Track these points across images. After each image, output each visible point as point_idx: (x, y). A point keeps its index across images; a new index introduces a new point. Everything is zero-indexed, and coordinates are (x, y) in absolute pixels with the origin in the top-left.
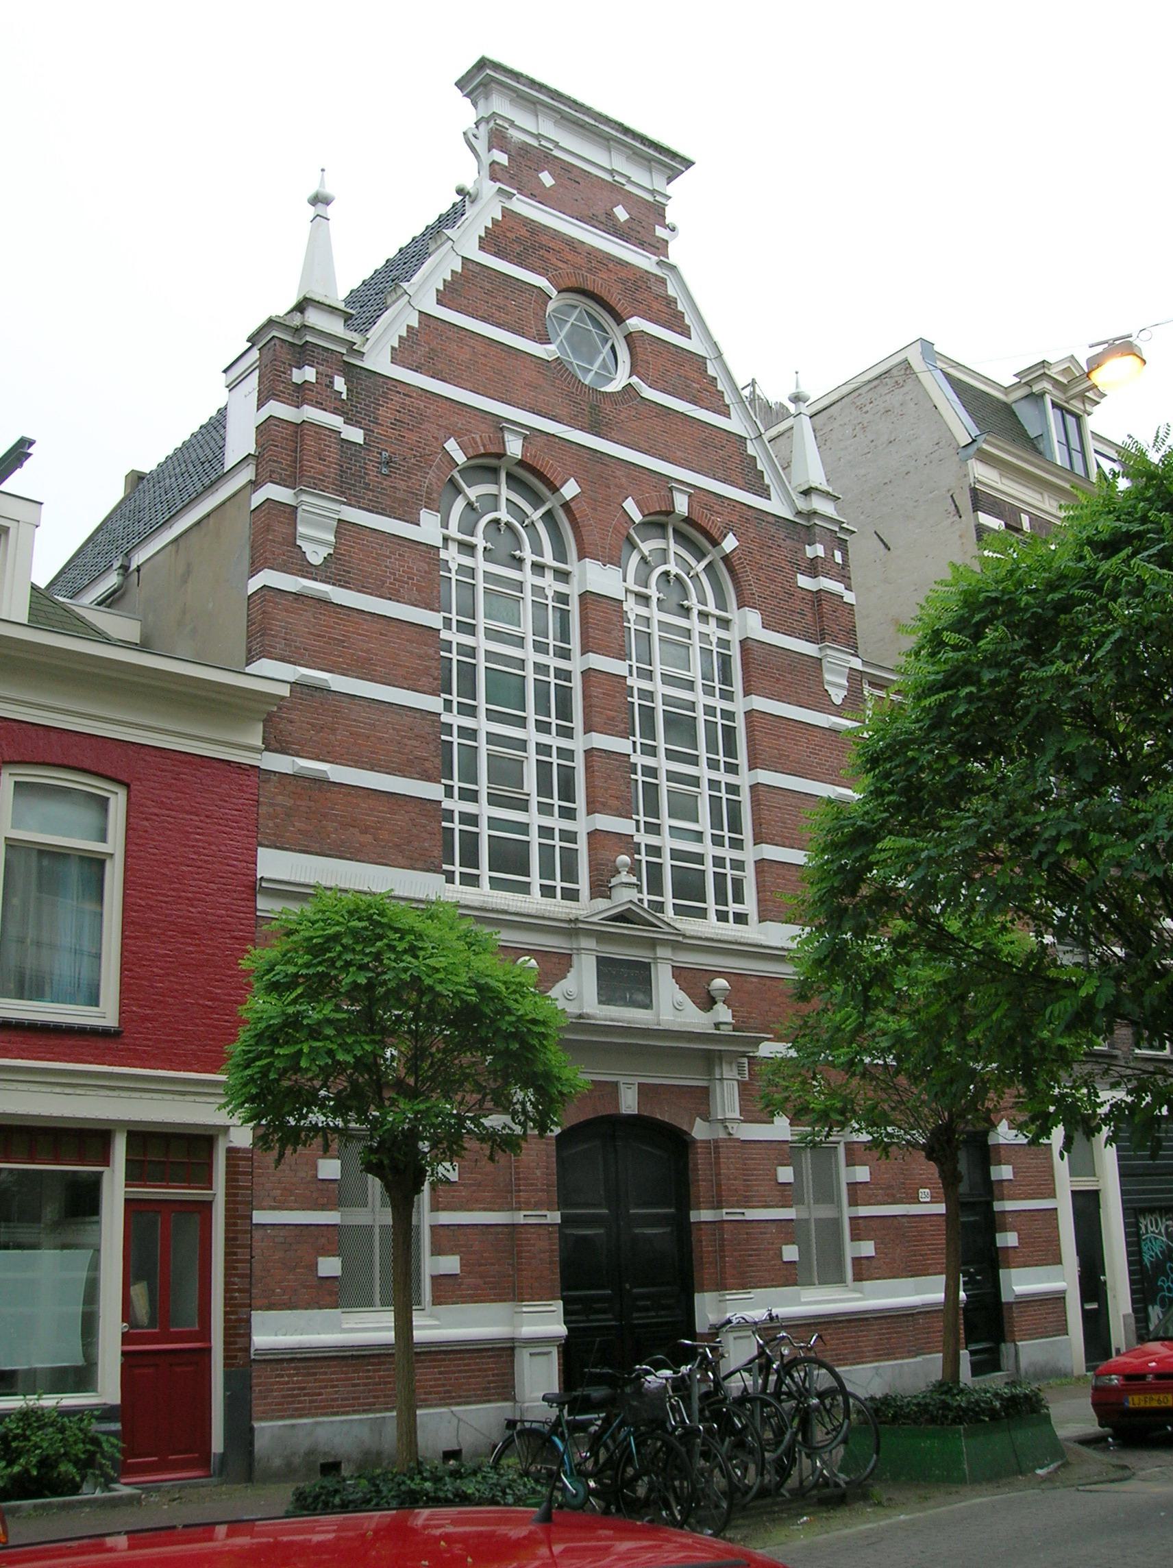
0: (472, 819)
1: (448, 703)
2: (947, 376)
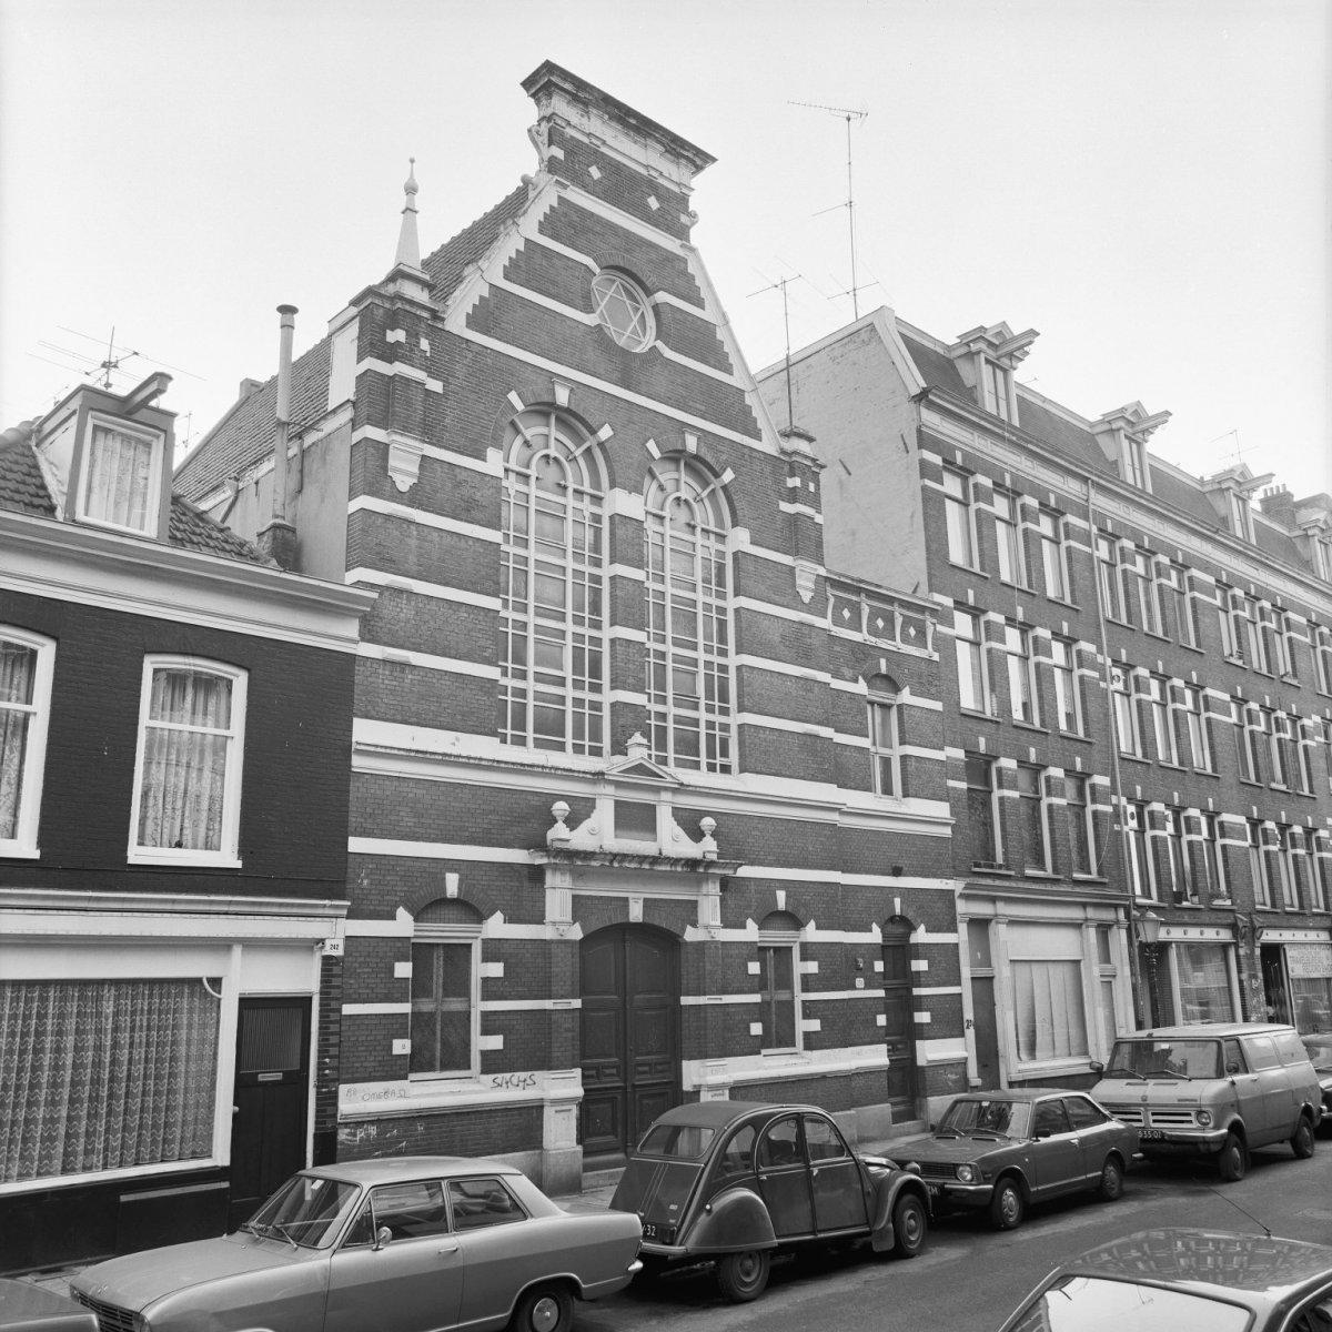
0: (522, 693)
1: (506, 601)
2: (903, 336)
